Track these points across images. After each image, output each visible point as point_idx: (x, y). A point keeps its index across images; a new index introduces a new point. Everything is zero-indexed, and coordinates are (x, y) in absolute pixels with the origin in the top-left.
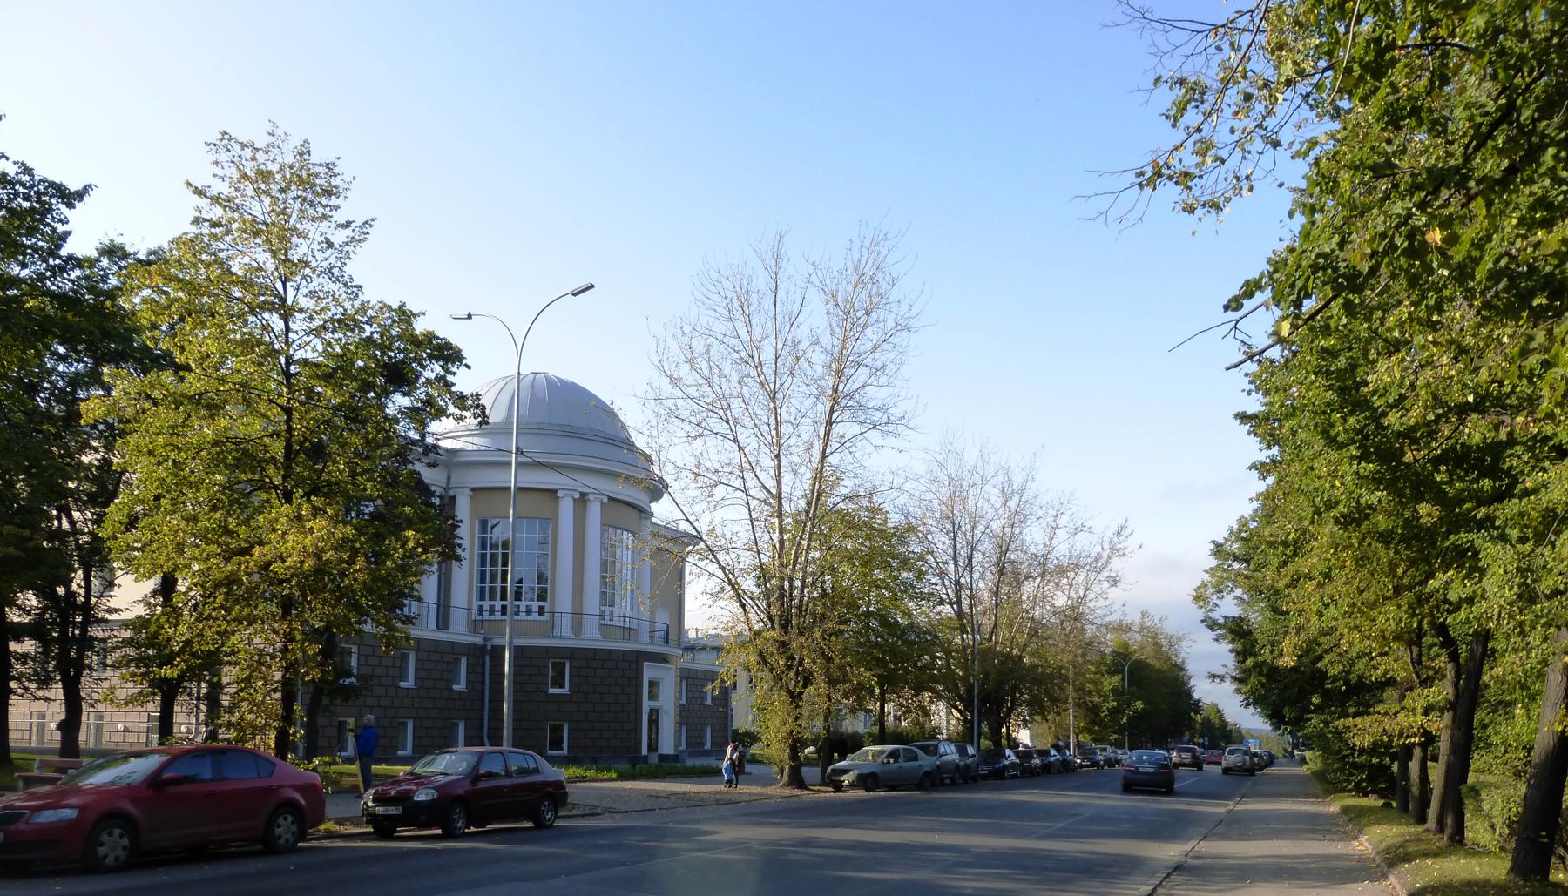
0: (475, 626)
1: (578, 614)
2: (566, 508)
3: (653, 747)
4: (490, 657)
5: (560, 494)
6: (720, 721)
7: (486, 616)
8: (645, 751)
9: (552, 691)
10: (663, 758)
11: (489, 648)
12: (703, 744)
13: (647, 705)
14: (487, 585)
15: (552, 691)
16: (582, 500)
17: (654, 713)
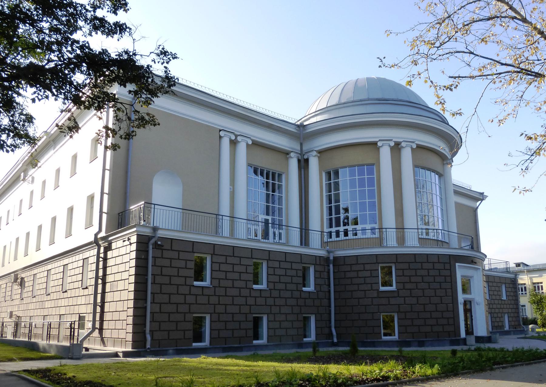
0: (324, 244)
1: (401, 228)
2: (385, 154)
3: (469, 331)
4: (333, 266)
5: (379, 144)
6: (514, 311)
7: (334, 238)
8: (463, 334)
9: (382, 289)
10: (479, 339)
11: (331, 258)
12: (503, 326)
13: (461, 297)
14: (334, 216)
15: (382, 289)
16: (397, 148)
17: (468, 304)
